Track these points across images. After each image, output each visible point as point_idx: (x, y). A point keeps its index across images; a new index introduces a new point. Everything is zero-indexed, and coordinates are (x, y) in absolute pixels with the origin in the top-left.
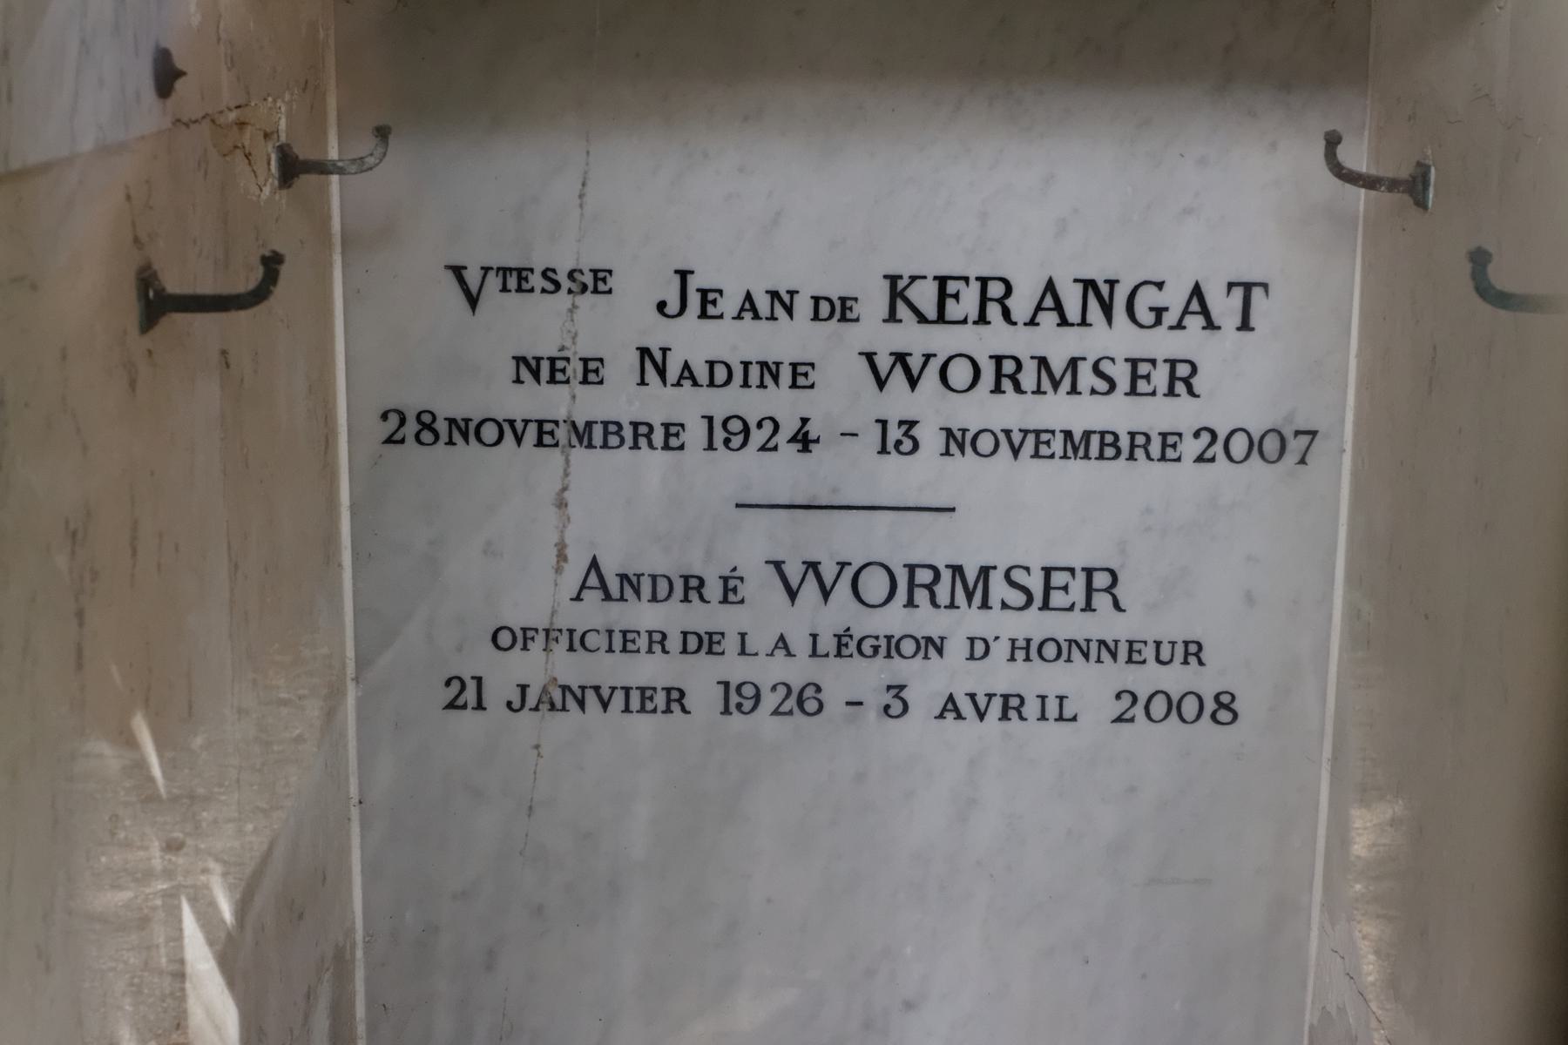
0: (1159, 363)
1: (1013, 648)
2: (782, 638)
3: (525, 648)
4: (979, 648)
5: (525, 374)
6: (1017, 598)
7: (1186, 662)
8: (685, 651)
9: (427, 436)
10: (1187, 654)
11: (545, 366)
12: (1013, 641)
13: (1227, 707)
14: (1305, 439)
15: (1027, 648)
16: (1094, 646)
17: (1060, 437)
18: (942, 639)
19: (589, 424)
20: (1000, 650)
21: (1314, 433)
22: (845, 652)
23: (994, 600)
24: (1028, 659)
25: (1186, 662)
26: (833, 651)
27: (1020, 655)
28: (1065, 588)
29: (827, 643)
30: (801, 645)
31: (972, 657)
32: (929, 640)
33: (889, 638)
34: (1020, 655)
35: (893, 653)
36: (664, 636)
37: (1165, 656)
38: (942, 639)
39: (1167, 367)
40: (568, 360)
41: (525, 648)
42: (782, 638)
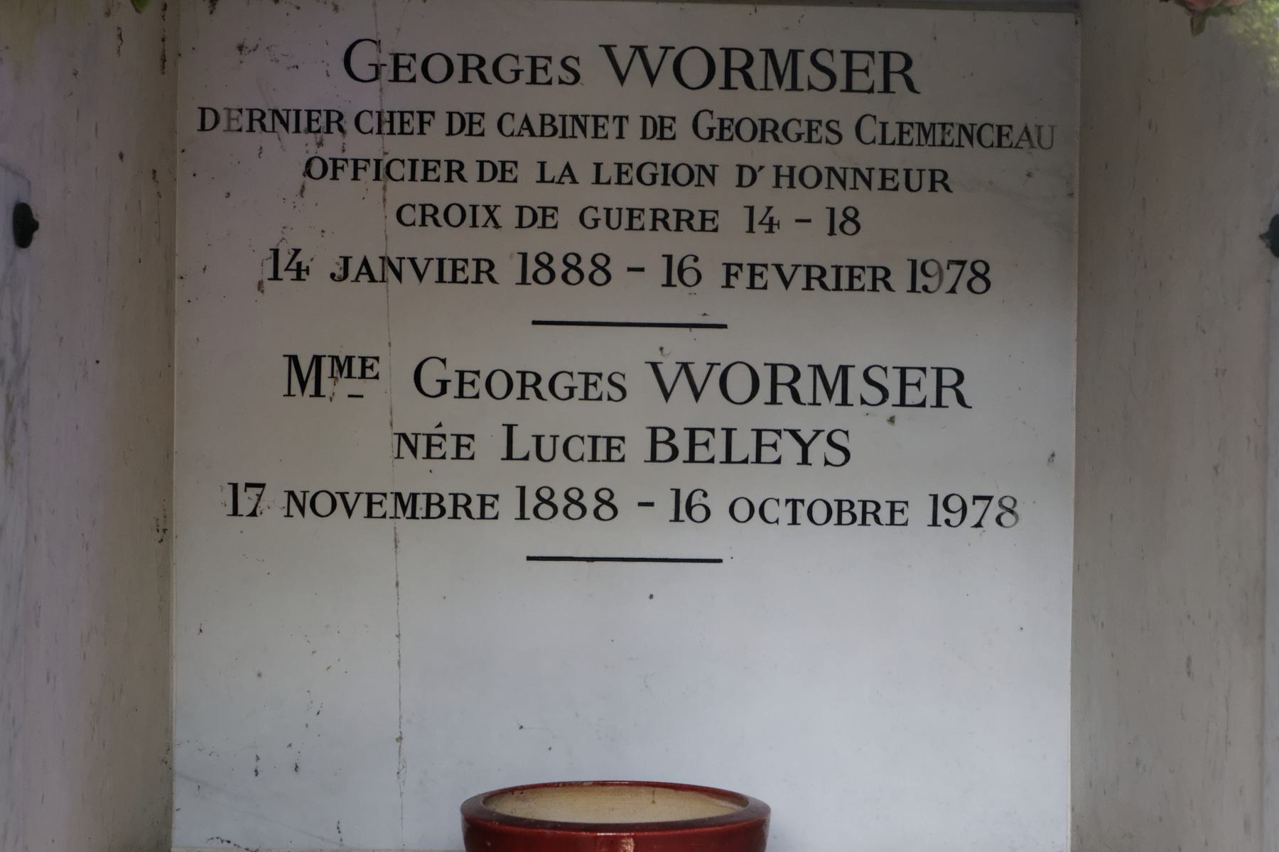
0: (928, 370)
1: (778, 176)
2: (568, 167)
3: (335, 178)
4: (747, 176)
5: (405, 450)
6: (822, 80)
7: (933, 189)
8: (481, 179)
9: (545, 510)
10: (933, 182)
11: (422, 441)
12: (778, 168)
13: (853, 220)
14: (253, 492)
15: (791, 176)
16: (850, 173)
17: (391, 498)
18: (714, 166)
19: (414, 496)
20: (766, 177)
21: (262, 486)
22: (625, 179)
23: (802, 83)
24: (792, 186)
25: (933, 189)
26: (615, 179)
27: (784, 182)
28: (409, 67)
29: (609, 172)
30: (585, 173)
31: (740, 185)
32: (702, 167)
33: (666, 166)
34: (784, 182)
35: (670, 180)
36: (462, 166)
37: (914, 183)
38: (714, 166)
39: (897, 373)
40: (444, 436)
41: (335, 178)
42: (568, 167)
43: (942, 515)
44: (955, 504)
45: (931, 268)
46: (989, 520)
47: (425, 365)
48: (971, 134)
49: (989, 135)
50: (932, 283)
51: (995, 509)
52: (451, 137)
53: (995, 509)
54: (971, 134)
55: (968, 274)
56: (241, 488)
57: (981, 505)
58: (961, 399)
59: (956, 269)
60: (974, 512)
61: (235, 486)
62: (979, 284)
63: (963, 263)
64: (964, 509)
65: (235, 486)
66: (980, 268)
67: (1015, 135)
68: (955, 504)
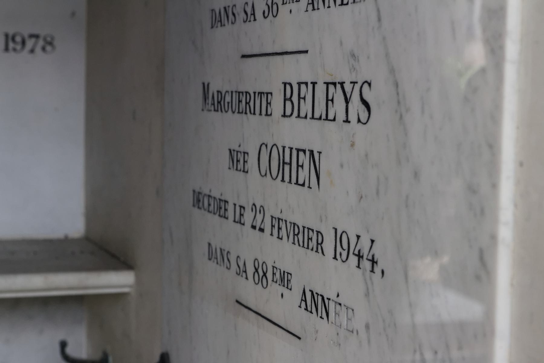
43: (11, 45)
44: (18, 39)
46: (38, 49)
51: (41, 43)
57: (33, 40)
60: (30, 44)
64: (24, 43)
68: (18, 39)
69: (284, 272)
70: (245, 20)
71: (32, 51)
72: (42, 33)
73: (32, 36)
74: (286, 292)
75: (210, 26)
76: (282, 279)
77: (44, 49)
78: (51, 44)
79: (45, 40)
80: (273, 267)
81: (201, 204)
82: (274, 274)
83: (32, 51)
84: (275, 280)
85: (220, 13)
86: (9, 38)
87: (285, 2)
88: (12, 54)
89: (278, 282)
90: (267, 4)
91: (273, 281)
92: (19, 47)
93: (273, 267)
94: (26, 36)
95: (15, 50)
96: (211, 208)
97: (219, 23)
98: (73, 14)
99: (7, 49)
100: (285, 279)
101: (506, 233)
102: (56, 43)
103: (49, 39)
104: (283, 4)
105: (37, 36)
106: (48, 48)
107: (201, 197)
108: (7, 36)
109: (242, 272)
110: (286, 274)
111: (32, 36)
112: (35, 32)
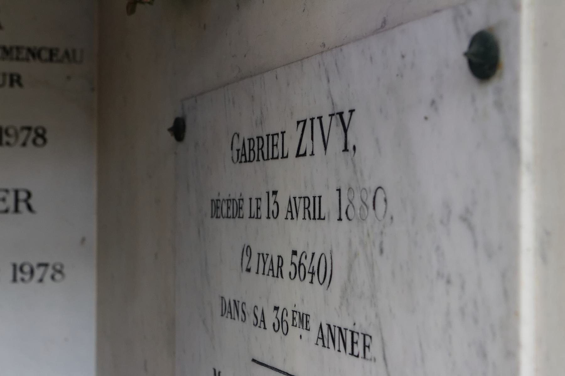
43: (19, 275)
44: (27, 269)
45: (11, 131)
46: (47, 278)
47: (384, 206)
48: (34, 54)
49: (45, 55)
50: (12, 140)
51: (50, 271)
52: (251, 219)
53: (50, 271)
54: (34, 54)
55: (33, 135)
56: (271, 194)
57: (42, 269)
58: (29, 208)
59: (25, 132)
60: (38, 272)
61: (268, 193)
62: (40, 141)
63: (29, 129)
64: (32, 272)
65: (268, 193)
66: (40, 131)
67: (61, 53)
68: (27, 269)
69: (303, 314)
70: (255, 323)
71: (41, 280)
72: (51, 262)
73: (40, 265)
74: (304, 333)
75: (220, 314)
76: (301, 321)
77: (53, 277)
78: (60, 272)
79: (54, 268)
80: (293, 311)
81: (219, 213)
82: (294, 319)
83: (41, 280)
84: (295, 324)
85: (230, 304)
86: (17, 269)
87: (301, 152)
88: (20, 284)
89: (298, 326)
90: (276, 317)
91: (293, 325)
92: (27, 277)
93: (293, 311)
94: (35, 265)
95: (23, 280)
96: (230, 213)
97: (229, 315)
98: (83, 240)
99: (15, 280)
100: (303, 320)
101: (527, 148)
102: (65, 271)
103: (58, 267)
104: (298, 155)
105: (46, 265)
106: (58, 276)
107: (219, 205)
108: (15, 266)
109: (260, 322)
110: (305, 316)
111: (40, 265)
112: (44, 261)
